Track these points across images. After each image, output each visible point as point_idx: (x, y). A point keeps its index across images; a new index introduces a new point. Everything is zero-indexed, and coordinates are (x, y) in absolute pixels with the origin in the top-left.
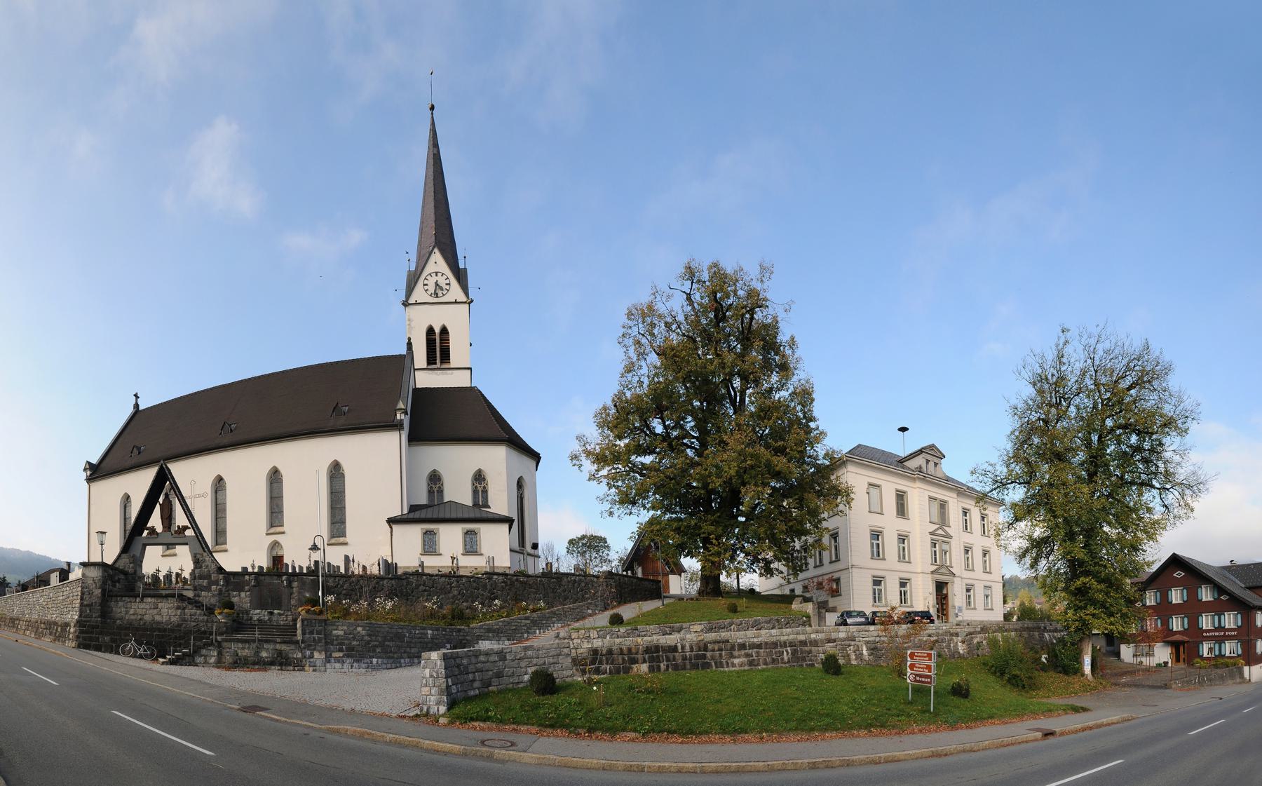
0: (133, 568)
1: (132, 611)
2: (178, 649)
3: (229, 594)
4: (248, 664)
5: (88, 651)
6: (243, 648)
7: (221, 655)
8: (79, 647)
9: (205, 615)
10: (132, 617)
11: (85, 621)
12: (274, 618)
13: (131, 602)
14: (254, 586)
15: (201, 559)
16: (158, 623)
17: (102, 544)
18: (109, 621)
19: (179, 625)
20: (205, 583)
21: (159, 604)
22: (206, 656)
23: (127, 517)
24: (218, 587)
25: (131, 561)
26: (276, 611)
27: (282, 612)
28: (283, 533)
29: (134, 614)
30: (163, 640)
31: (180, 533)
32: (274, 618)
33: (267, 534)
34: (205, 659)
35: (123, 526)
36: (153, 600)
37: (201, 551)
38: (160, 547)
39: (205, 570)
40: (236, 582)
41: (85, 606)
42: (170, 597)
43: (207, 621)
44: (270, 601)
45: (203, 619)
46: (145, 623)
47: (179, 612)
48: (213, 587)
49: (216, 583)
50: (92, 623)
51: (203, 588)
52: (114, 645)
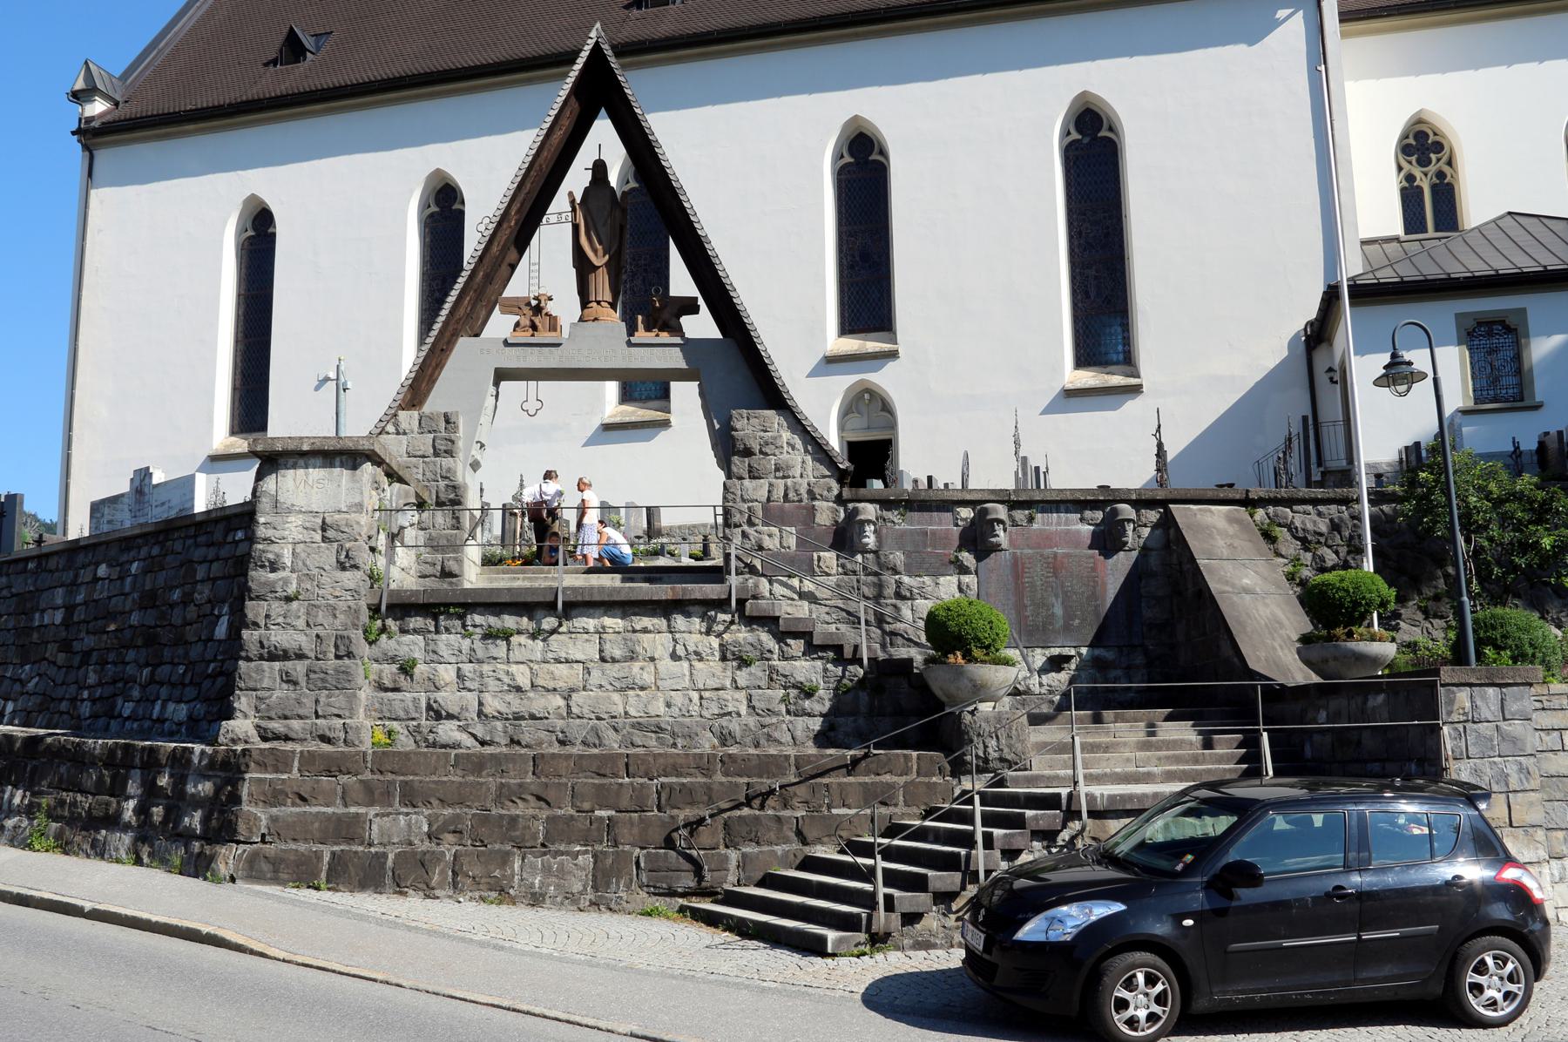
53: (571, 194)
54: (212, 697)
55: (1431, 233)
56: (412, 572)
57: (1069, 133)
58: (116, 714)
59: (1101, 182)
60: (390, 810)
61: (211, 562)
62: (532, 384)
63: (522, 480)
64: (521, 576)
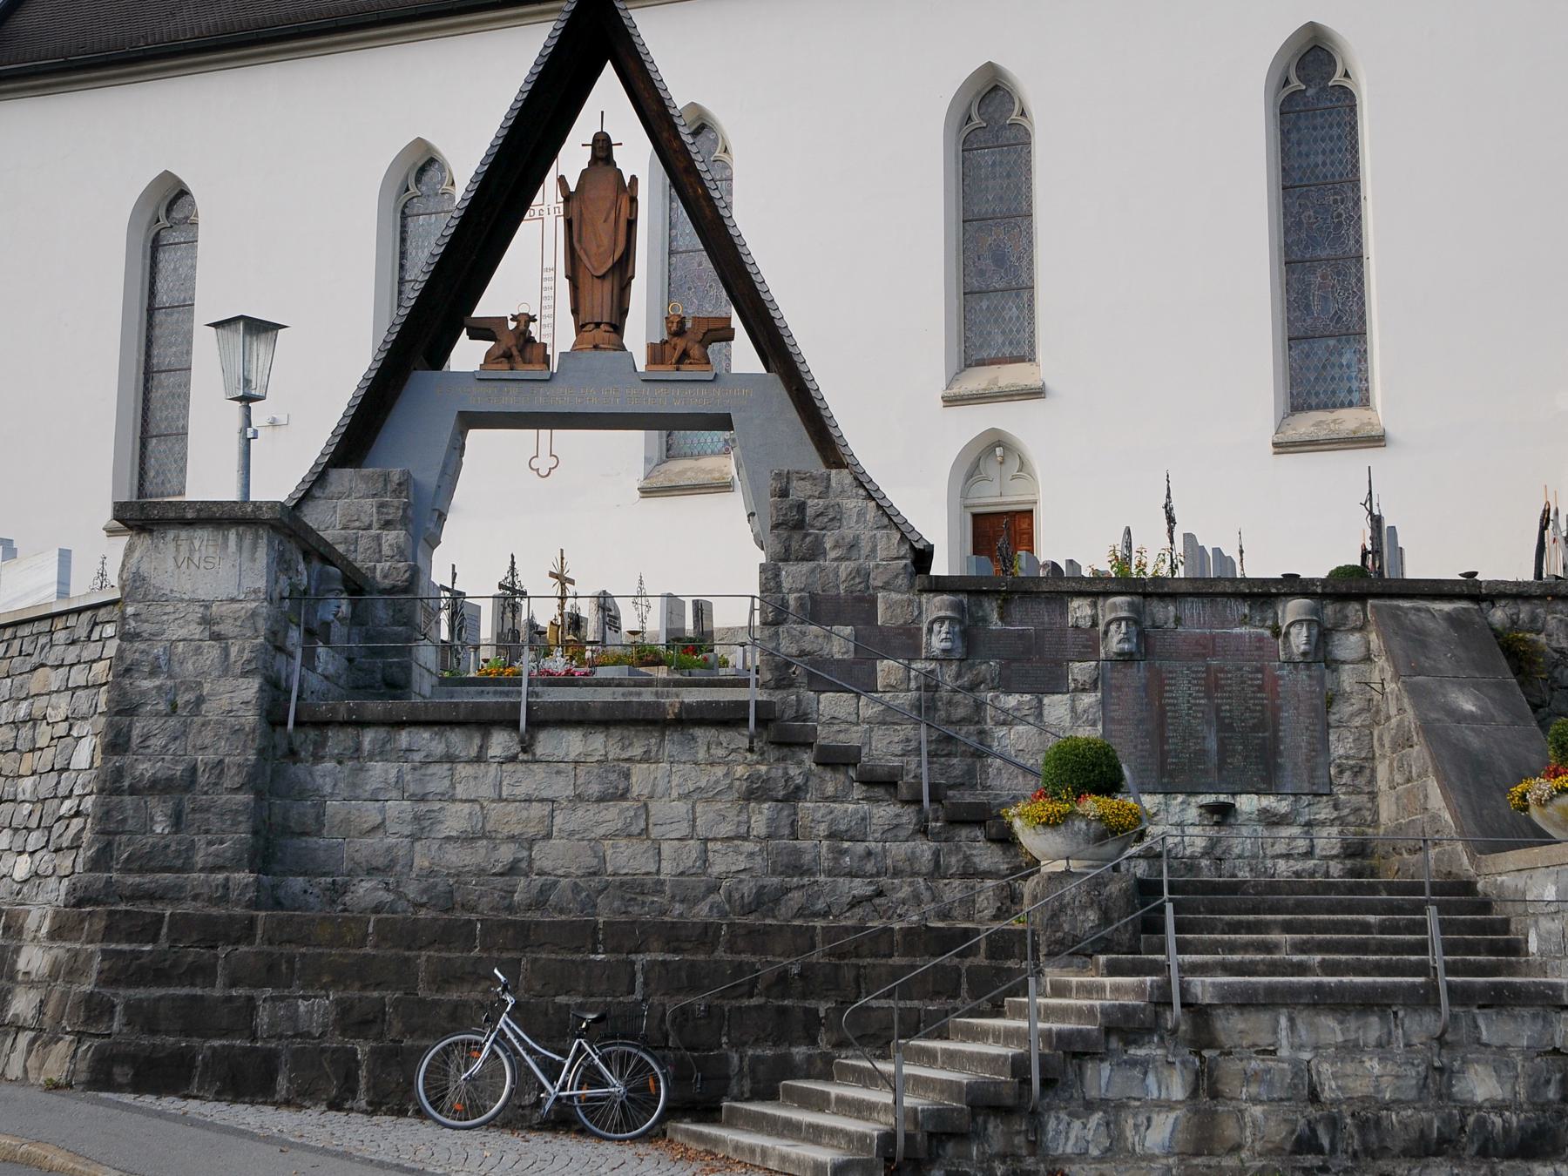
0: (401, 553)
1: (455, 819)
2: (799, 1052)
3: (979, 706)
4: (1384, 1151)
5: (170, 1104)
6: (1350, 1049)
7: (1215, 1095)
8: (101, 1077)
9: (923, 830)
10: (457, 857)
11: (137, 895)
12: (1241, 840)
13: (450, 759)
14: (1125, 658)
15: (813, 506)
16: (633, 888)
17: (247, 399)
18: (298, 883)
19: (764, 901)
20: (838, 643)
21: (638, 771)
22: (1113, 1109)
23: (163, 298)
24: (917, 665)
25: (392, 514)
26: (1247, 803)
27: (1283, 806)
28: (1037, 393)
29: (467, 839)
30: (699, 1001)
31: (684, 356)
32: (1241, 840)
33: (950, 401)
34: (1112, 1126)
35: (136, 356)
36: (601, 743)
37: (811, 460)
38: (635, 441)
39: (838, 572)
40: (1021, 635)
41: (133, 790)
42: (702, 722)
43: (937, 871)
44: (1212, 744)
45: (912, 858)
46: (545, 891)
47: (761, 817)
48: (888, 669)
49: (906, 642)
50: (188, 907)
51: (824, 675)
52: (362, 1049)
53: (562, 180)
54: (64, 845)
55: (1429, 936)
56: (342, 682)
57: (1287, 82)
58: (947, 623)
59: (1332, 151)
60: (286, 992)
61: (72, 665)
62: (545, 433)
63: (513, 563)
64: (491, 689)
